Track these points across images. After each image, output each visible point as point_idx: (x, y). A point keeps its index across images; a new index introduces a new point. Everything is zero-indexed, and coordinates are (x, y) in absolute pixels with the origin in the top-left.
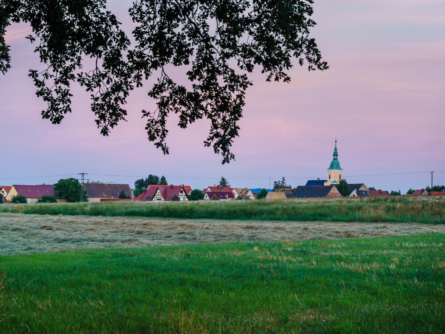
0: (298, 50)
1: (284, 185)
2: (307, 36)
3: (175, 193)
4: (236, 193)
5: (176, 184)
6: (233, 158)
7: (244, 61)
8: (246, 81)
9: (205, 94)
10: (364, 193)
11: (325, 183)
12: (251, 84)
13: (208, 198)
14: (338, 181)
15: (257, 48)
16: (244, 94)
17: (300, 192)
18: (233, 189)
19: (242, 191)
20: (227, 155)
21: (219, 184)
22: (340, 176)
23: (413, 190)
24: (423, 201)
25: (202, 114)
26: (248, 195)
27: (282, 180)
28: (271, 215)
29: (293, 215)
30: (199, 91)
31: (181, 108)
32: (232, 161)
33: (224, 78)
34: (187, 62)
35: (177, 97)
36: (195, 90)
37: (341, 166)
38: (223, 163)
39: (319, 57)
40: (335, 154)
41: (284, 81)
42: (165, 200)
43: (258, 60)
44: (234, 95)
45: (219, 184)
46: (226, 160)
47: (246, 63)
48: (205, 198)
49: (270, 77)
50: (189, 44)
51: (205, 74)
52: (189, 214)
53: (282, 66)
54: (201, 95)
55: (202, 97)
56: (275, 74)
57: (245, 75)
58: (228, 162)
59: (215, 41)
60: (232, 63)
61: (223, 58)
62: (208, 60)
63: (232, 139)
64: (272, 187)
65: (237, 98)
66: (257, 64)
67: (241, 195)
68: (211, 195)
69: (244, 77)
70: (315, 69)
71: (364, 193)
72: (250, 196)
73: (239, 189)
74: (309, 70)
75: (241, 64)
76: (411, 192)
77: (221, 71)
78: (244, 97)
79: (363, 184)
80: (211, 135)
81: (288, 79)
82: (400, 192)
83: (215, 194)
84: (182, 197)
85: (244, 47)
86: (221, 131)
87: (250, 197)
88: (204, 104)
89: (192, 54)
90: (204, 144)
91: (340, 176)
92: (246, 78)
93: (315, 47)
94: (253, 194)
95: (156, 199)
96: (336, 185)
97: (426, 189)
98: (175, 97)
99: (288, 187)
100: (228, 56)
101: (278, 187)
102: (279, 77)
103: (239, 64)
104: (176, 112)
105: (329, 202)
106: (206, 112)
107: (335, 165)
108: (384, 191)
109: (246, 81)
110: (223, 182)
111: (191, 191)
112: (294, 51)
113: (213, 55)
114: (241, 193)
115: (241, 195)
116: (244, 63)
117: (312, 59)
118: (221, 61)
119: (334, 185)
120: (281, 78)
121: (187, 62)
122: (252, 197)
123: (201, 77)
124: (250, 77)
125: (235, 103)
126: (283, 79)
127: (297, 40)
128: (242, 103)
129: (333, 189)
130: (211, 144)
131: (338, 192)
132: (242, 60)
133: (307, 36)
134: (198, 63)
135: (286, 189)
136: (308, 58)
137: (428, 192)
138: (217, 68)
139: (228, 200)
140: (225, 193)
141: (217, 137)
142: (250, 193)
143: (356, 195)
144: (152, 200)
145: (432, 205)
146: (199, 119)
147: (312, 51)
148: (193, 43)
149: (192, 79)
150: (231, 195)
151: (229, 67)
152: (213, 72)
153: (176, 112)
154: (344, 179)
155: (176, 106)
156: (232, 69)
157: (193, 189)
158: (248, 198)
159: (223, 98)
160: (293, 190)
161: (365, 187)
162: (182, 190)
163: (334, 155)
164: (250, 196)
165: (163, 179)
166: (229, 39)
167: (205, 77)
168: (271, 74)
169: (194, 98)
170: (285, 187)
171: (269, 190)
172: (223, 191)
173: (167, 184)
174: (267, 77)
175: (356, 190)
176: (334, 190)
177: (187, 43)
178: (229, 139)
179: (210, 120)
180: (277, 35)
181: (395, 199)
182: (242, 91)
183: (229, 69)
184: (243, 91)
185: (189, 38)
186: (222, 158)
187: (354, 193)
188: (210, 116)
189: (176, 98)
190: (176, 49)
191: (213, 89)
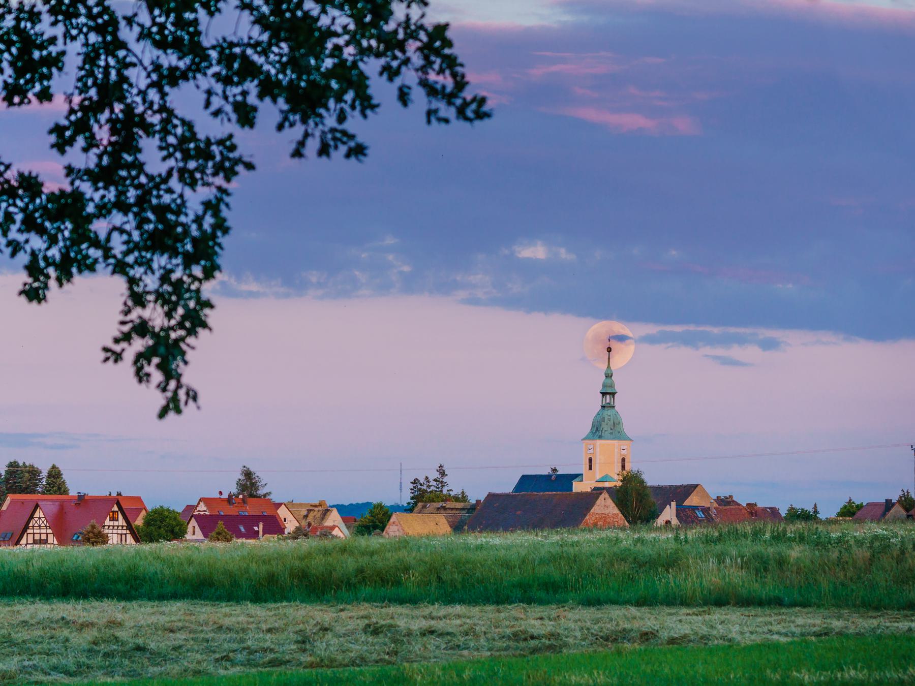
0: (395, 58)
1: (445, 492)
2: (423, 16)
3: (93, 522)
4: (290, 517)
5: (94, 490)
6: (195, 398)
7: (224, 92)
8: (231, 155)
9: (103, 197)
10: (700, 514)
11: (574, 484)
12: (250, 166)
13: (199, 535)
14: (616, 477)
15: (265, 53)
16: (228, 194)
17: (493, 513)
18: (280, 505)
19: (309, 511)
20: (175, 392)
21: (234, 490)
22: (623, 460)
23: (858, 502)
24: (876, 537)
25: (96, 261)
26: (328, 523)
27: (437, 475)
28: (385, 583)
29: (459, 586)
30: (86, 187)
31: (27, 241)
32: (189, 409)
33: (161, 148)
34: (45, 96)
35: (15, 205)
36: (72, 183)
37: (627, 427)
38: (163, 413)
39: (460, 84)
40: (608, 393)
41: (348, 156)
42: (61, 543)
43: (268, 88)
44: (196, 198)
45: (234, 490)
46: (172, 406)
47: (231, 99)
48: (188, 536)
49: (302, 144)
50: (53, 40)
51: (103, 134)
52: (127, 585)
53: (347, 107)
54: (92, 200)
55: (97, 206)
56: (317, 133)
57: (230, 137)
58: (178, 411)
59: (137, 29)
60: (186, 100)
61: (157, 85)
62: (111, 91)
63: (191, 340)
64: (406, 498)
65: (205, 213)
66: (268, 100)
67: (304, 523)
68: (208, 525)
69: (228, 144)
70: (446, 121)
71: (700, 514)
72: (333, 528)
73: (301, 505)
74: (429, 122)
75: (217, 102)
76: (850, 512)
77: (152, 125)
78: (227, 205)
79: (697, 486)
80: (126, 328)
81: (358, 151)
82: (816, 512)
83: (220, 523)
84: (116, 535)
85: (226, 51)
86: (155, 315)
87: (336, 532)
88: (100, 227)
89: (60, 69)
90: (103, 355)
91: (623, 460)
92: (233, 148)
93: (447, 51)
94: (345, 520)
95: (30, 541)
96: (609, 490)
97: (899, 501)
98: (9, 205)
99: (456, 499)
100: (174, 77)
101: (424, 498)
102: (332, 143)
103: (208, 104)
104: (13, 254)
105: (577, 543)
106: (107, 252)
107: (604, 426)
108: (764, 509)
109: (231, 155)
110: (249, 483)
111: (143, 513)
112: (382, 61)
113: (131, 73)
114: (306, 516)
115: (304, 523)
116: (226, 98)
117: (439, 87)
118: (153, 95)
119: (604, 488)
120: (336, 147)
121: (45, 96)
122: (341, 532)
123: (91, 143)
124: (247, 142)
125: (200, 226)
126: (343, 149)
127: (390, 27)
128: (221, 226)
129: (600, 501)
130: (125, 355)
131: (616, 511)
132: (220, 91)
133: (423, 16)
134: (85, 99)
135: (449, 505)
136: (424, 83)
137: (907, 510)
138: (142, 115)
139: (267, 543)
140: (256, 519)
141: (143, 336)
142: (334, 518)
143: (675, 522)
144: (17, 543)
145: (903, 552)
146: (86, 273)
147: (438, 61)
148: (65, 37)
149: (61, 146)
150: (274, 526)
151: (177, 112)
152: (128, 128)
153: (13, 254)
154: (635, 469)
155: (13, 234)
156: (188, 118)
157: (151, 504)
158: (327, 533)
159: (161, 211)
160: (472, 508)
161: (705, 495)
162: (116, 508)
163: (604, 394)
164: (333, 528)
165: (55, 474)
166: (180, 23)
167: (105, 142)
168: (306, 135)
169: (68, 206)
170: (447, 498)
171: (397, 508)
172: (250, 510)
173: (66, 492)
174: (294, 146)
175: (673, 504)
176: (606, 507)
177: (45, 37)
178: (182, 339)
179: (120, 283)
180: (324, 11)
181: (785, 531)
182: (219, 189)
183: (176, 117)
184: (225, 185)
185: (53, 19)
186: (160, 400)
187: (669, 513)
188: (120, 268)
189: (12, 209)
190: (11, 54)
191: (128, 182)
